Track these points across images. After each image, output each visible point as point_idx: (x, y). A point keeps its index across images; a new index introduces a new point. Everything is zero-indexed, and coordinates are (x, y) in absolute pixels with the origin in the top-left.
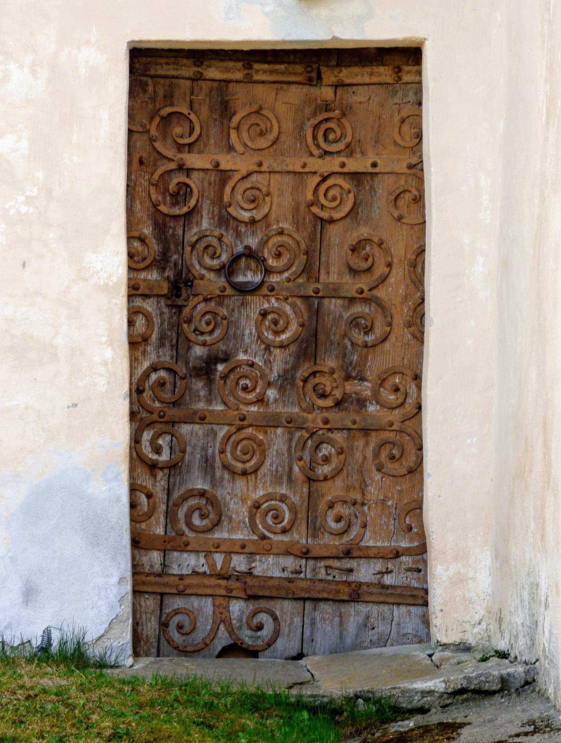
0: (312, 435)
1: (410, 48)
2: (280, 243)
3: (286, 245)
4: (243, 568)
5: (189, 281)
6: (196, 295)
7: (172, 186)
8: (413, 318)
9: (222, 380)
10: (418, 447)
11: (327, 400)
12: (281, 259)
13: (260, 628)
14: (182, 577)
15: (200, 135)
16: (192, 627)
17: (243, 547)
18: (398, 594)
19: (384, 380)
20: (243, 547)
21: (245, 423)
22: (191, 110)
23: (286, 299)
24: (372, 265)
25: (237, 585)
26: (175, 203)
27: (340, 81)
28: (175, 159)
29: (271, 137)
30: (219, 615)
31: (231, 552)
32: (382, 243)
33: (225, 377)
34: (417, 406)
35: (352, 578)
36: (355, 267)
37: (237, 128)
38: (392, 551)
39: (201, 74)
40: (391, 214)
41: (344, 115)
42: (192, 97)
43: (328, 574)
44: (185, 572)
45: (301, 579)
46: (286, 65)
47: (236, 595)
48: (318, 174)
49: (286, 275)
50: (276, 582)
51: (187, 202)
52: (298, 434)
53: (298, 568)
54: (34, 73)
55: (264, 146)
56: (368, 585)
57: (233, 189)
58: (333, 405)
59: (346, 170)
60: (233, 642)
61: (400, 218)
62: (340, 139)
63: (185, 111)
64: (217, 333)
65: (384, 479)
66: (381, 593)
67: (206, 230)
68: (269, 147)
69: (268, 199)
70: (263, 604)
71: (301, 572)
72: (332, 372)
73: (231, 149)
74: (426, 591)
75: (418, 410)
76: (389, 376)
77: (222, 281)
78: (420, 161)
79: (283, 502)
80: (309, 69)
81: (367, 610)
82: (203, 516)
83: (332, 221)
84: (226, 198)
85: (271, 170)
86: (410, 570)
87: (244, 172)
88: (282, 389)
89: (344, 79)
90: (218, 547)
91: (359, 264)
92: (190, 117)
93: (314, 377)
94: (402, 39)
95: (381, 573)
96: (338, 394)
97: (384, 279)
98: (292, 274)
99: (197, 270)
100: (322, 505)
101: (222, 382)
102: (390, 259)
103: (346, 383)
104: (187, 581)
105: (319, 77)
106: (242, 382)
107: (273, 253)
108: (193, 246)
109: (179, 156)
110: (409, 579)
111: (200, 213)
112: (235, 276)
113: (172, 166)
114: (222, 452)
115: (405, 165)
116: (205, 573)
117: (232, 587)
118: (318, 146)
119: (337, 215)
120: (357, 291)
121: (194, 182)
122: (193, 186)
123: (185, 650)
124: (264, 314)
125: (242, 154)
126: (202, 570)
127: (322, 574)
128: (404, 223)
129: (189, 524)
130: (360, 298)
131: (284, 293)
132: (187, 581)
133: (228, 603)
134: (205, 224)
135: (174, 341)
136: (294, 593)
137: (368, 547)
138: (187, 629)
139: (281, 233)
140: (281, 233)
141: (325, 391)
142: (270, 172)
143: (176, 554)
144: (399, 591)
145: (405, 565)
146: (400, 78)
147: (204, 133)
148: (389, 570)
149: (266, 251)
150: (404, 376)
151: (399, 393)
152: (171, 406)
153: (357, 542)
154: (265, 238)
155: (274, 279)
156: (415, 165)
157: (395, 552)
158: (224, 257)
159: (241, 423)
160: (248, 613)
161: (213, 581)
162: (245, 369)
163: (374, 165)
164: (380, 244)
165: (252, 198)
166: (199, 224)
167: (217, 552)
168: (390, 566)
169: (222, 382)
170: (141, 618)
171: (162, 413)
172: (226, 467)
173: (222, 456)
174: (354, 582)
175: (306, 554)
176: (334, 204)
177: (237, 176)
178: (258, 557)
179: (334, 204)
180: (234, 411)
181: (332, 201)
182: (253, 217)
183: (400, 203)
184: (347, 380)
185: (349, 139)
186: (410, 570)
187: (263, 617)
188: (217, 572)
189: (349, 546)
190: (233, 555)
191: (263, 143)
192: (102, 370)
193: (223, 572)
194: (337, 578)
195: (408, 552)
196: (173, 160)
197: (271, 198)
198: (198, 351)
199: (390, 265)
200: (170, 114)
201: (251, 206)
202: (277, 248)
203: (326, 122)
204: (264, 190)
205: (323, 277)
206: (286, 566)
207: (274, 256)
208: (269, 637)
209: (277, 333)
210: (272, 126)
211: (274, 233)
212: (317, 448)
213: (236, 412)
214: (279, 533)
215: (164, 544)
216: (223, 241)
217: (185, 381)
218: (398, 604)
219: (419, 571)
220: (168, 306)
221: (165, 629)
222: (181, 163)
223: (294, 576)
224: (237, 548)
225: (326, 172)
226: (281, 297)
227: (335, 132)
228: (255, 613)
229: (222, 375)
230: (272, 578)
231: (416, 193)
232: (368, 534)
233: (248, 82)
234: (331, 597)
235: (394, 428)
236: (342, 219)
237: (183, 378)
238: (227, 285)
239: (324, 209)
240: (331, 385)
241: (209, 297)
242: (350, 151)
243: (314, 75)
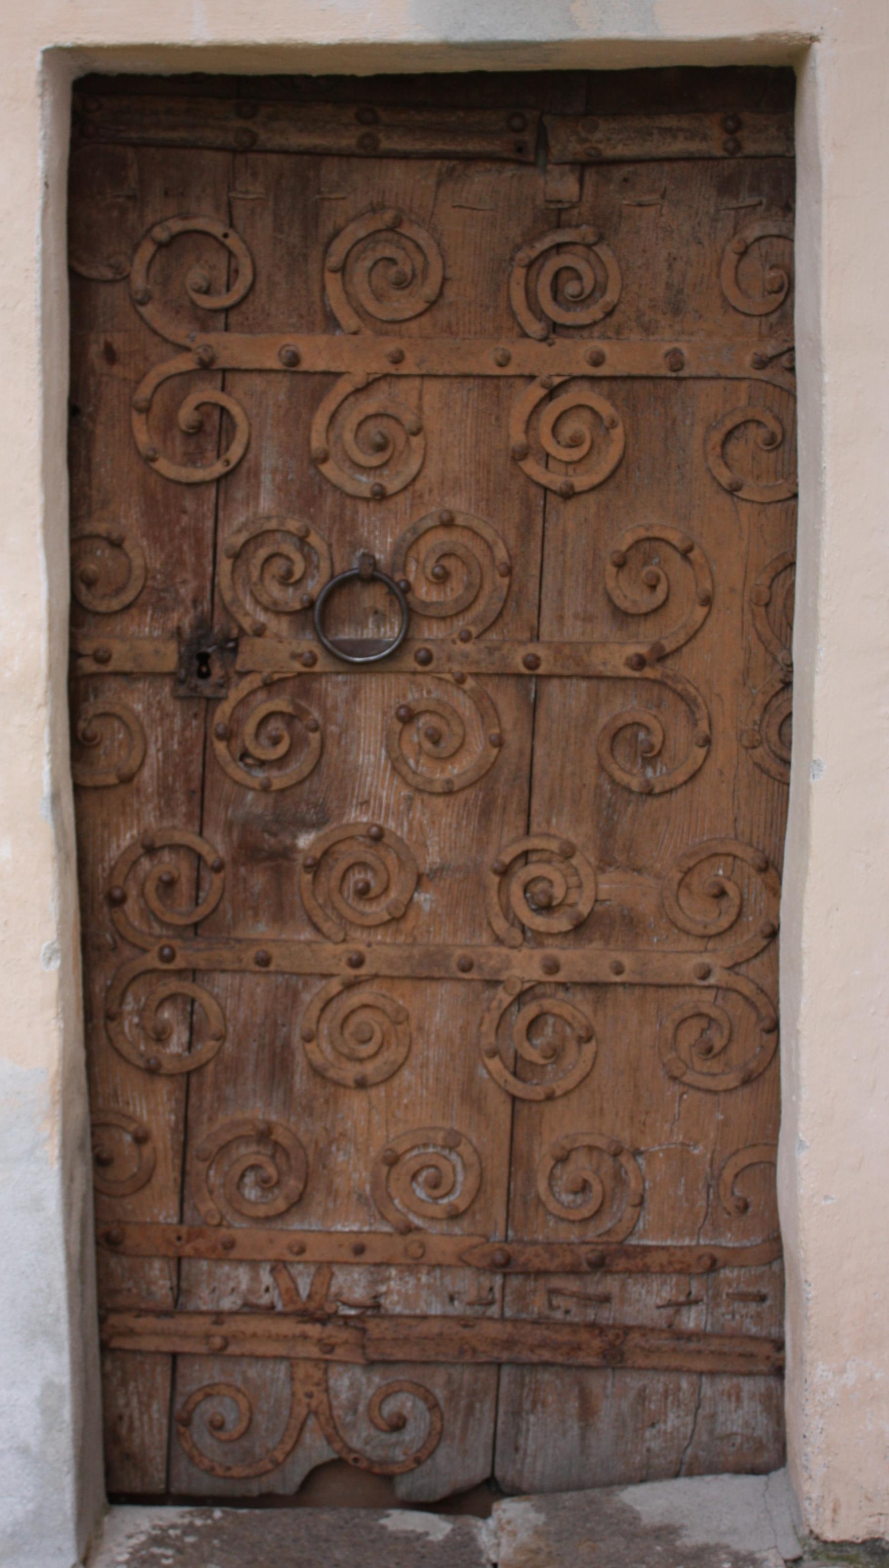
1: (766, 68)
2: (446, 549)
3: (461, 551)
4: (359, 1294)
5: (228, 640)
6: (243, 674)
7: (186, 415)
8: (760, 726)
9: (309, 873)
10: (767, 1024)
11: (556, 915)
12: (449, 585)
13: (398, 1425)
14: (219, 1317)
15: (252, 288)
16: (244, 1424)
17: (359, 1250)
18: (712, 1352)
19: (688, 871)
20: (359, 1250)
21: (363, 971)
22: (232, 225)
23: (460, 680)
24: (666, 600)
25: (344, 1335)
26: (192, 459)
27: (593, 152)
28: (193, 346)
29: (429, 290)
30: (305, 1400)
31: (330, 1263)
32: (690, 549)
33: (316, 867)
34: (768, 930)
35: (606, 1315)
36: (625, 605)
37: (342, 269)
38: (700, 1257)
39: (254, 137)
40: (714, 478)
41: (601, 238)
42: (232, 194)
43: (551, 1306)
44: (227, 1303)
45: (491, 1318)
46: (461, 114)
47: (344, 1358)
48: (538, 380)
49: (460, 623)
50: (434, 1328)
51: (222, 452)
53: (484, 1293)
55: (408, 314)
56: (644, 1330)
57: (333, 417)
58: (570, 927)
59: (603, 371)
60: (334, 1456)
61: (733, 490)
62: (590, 296)
63: (218, 229)
65: (685, 1096)
66: (674, 1350)
67: (268, 518)
68: (421, 314)
69: (415, 441)
71: (491, 1303)
72: (568, 853)
74: (779, 1345)
75: (764, 942)
76: (701, 861)
77: (307, 643)
78: (786, 346)
79: (451, 1149)
80: (517, 122)
81: (641, 1384)
82: (265, 1184)
83: (569, 494)
84: (317, 442)
85: (424, 372)
86: (743, 1297)
87: (359, 379)
89: (601, 146)
90: (302, 1251)
92: (228, 242)
93: (526, 863)
94: (752, 39)
95: (677, 1306)
98: (474, 623)
99: (247, 614)
101: (309, 877)
102: (708, 586)
103: (602, 878)
104: (232, 1326)
105: (543, 144)
106: (357, 877)
107: (428, 571)
108: (236, 556)
109: (203, 339)
110: (737, 1317)
111: (255, 473)
112: (333, 632)
113: (185, 363)
115: (748, 359)
116: (272, 1307)
117: (333, 1340)
118: (539, 314)
119: (581, 482)
120: (290, 1248)
121: (239, 402)
122: (235, 410)
123: (229, 1474)
124: (408, 717)
125: (355, 333)
126: (265, 1300)
128: (743, 499)
130: (635, 679)
131: (456, 668)
132: (232, 1326)
133: (326, 1372)
134: (266, 503)
135: (196, 784)
136: (474, 1350)
137: (647, 1249)
138: (233, 1427)
140: (448, 523)
141: (551, 898)
142: (422, 376)
143: (204, 1265)
144: (715, 1345)
145: (730, 1286)
146: (739, 146)
147: (261, 285)
148: (692, 1297)
149: (412, 567)
150: (738, 862)
151: (724, 903)
152: (190, 933)
153: (620, 1237)
154: (409, 537)
156: (772, 359)
157: (707, 1261)
158: (314, 587)
159: (352, 972)
160: (371, 1392)
161: (288, 1327)
162: (360, 851)
164: (685, 554)
165: (378, 439)
166: (253, 496)
167: (299, 1262)
168: (695, 1287)
169: (309, 877)
170: (127, 1405)
171: (167, 951)
173: (310, 1047)
174: (613, 1327)
176: (575, 454)
177: (343, 387)
178: (393, 1272)
179: (575, 454)
180: (336, 943)
181: (571, 447)
182: (381, 486)
183: (736, 449)
184: (603, 871)
185: (611, 296)
186: (743, 1297)
188: (299, 1306)
189: (600, 1247)
190: (335, 1269)
193: (312, 1306)
194: (575, 1317)
195: (735, 1256)
196: (188, 349)
197: (425, 439)
199: (707, 601)
200: (175, 238)
201: (375, 460)
202: (438, 561)
203: (558, 253)
204: (409, 419)
206: (456, 1289)
207: (431, 578)
208: (418, 1445)
210: (426, 264)
211: (430, 523)
213: (342, 947)
214: (441, 1220)
215: (178, 1244)
216: (309, 544)
217: (222, 874)
218: (713, 1374)
219: (762, 1298)
220: (177, 697)
221: (182, 1429)
222: (206, 358)
223: (478, 1309)
224: (346, 1254)
225: (558, 375)
226: (448, 677)
227: (579, 278)
228: (386, 1394)
229: (309, 862)
230: (424, 1317)
231: (773, 425)
233: (368, 157)
234: (560, 1359)
235: (712, 981)
236: (593, 489)
237: (218, 869)
238: (318, 651)
239: (552, 464)
240: (566, 882)
241: (276, 677)
243: (529, 137)
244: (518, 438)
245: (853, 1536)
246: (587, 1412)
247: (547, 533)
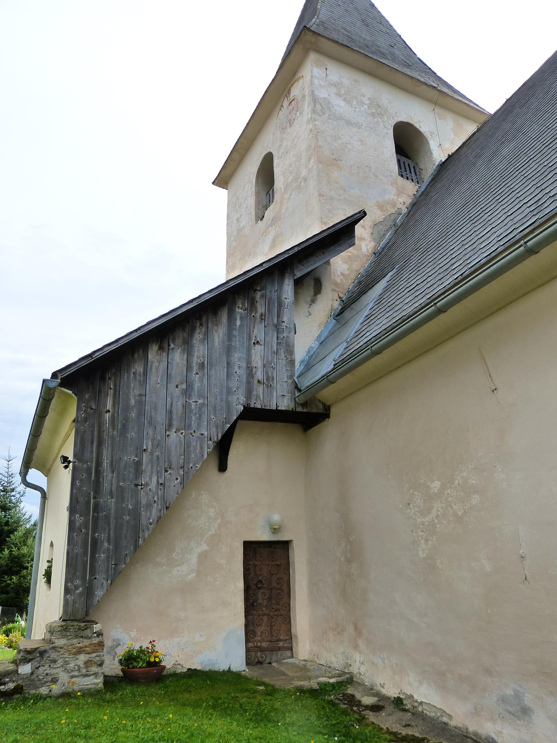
0: (271, 617)
4: (260, 645)
25: (259, 649)
33: (256, 606)
35: (279, 645)
52: (269, 617)
54: (227, 547)
56: (281, 646)
64: (255, 597)
70: (263, 652)
72: (274, 604)
73: (257, 560)
77: (255, 587)
82: (252, 635)
88: (265, 608)
91: (279, 582)
96: (276, 608)
97: (283, 585)
100: (273, 631)
114: (256, 621)
124: (263, 593)
127: (273, 645)
129: (250, 637)
132: (250, 649)
139: (265, 576)
155: (264, 586)
161: (254, 648)
163: (281, 563)
172: (256, 624)
175: (271, 641)
187: (264, 655)
191: (262, 559)
192: (240, 607)
198: (251, 601)
205: (272, 585)
209: (265, 596)
212: (272, 619)
232: (281, 636)
242: (276, 560)
244: (270, 569)
245: (116, 674)
246: (277, 655)
247: (545, 172)
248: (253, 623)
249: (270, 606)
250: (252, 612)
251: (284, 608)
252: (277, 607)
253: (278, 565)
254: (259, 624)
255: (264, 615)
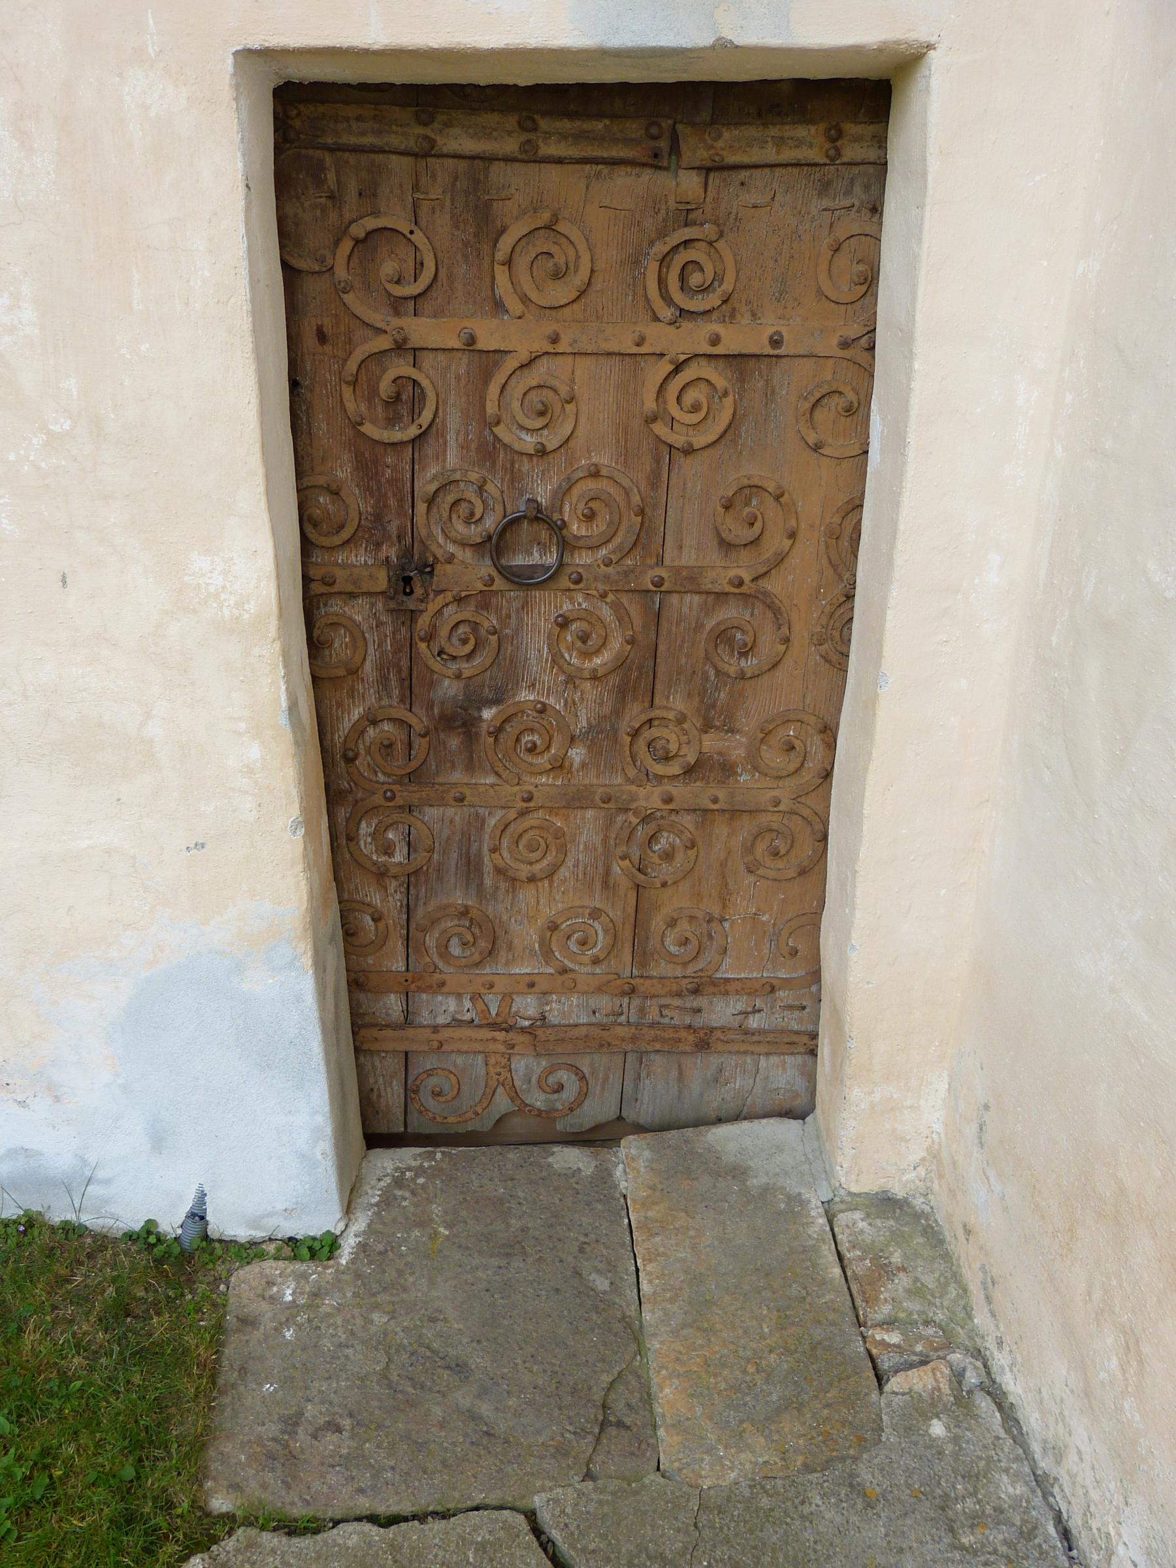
33: (497, 732)
77: (486, 568)
88: (593, 748)
91: (740, 533)
97: (780, 559)
100: (657, 923)
114: (494, 850)
124: (564, 623)
132: (445, 1034)
155: (583, 559)
161: (486, 1034)
163: (776, 342)
191: (560, 293)
209: (587, 655)
212: (653, 838)
242: (728, 308)
244: (650, 405)
248: (471, 868)
249: (635, 734)
250: (457, 776)
251: (773, 758)
252: (711, 743)
253: (737, 361)
254: (524, 871)
255: (577, 800)
